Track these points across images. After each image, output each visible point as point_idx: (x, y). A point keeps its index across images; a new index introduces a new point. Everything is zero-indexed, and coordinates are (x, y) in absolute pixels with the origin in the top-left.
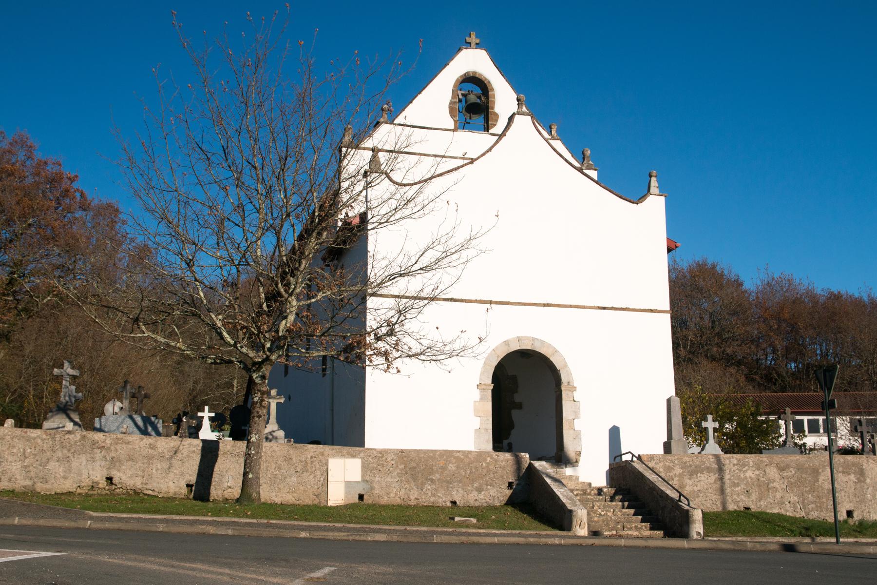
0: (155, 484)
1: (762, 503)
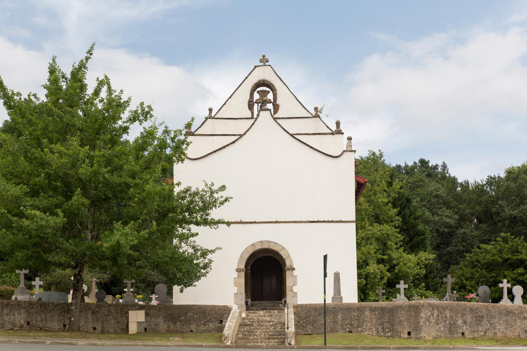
0: (49, 325)
1: (359, 329)
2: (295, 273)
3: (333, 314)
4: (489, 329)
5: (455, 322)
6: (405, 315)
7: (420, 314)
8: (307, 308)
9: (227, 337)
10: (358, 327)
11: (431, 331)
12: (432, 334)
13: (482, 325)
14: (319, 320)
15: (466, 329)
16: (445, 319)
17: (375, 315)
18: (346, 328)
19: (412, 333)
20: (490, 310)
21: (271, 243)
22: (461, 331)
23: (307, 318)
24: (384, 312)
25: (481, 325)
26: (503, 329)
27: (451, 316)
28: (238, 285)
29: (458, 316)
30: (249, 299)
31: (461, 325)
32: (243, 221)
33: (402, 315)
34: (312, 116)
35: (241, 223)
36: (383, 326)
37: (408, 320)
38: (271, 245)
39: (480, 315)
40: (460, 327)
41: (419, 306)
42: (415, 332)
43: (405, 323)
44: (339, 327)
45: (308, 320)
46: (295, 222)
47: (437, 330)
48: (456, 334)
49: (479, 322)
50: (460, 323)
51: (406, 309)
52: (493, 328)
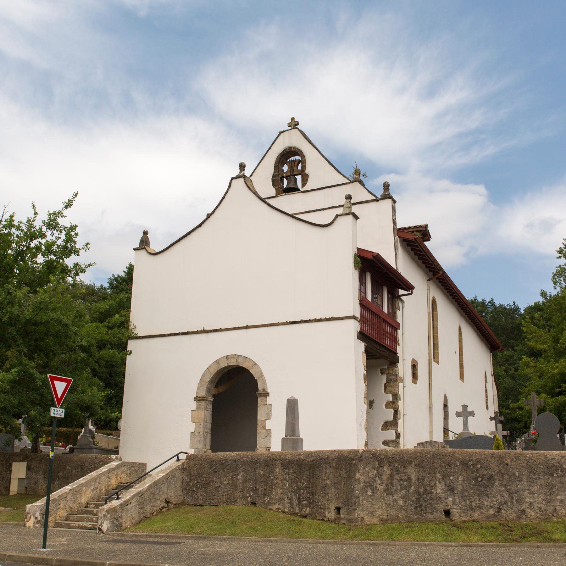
2: (269, 400)
3: (232, 472)
4: (506, 503)
5: (428, 488)
6: (331, 475)
7: (355, 474)
8: (201, 460)
9: (28, 513)
10: (265, 495)
11: (376, 506)
12: (379, 512)
13: (491, 494)
14: (213, 481)
15: (454, 503)
16: (405, 483)
17: (289, 475)
18: (248, 497)
19: (342, 511)
20: (507, 465)
21: (240, 357)
22: (442, 507)
23: (199, 477)
24: (301, 469)
25: (487, 495)
26: (540, 503)
27: (420, 477)
28: (197, 421)
29: (435, 477)
31: (442, 495)
32: (206, 329)
33: (327, 475)
34: (349, 181)
35: (204, 332)
36: (300, 495)
37: (336, 485)
38: (239, 361)
39: (484, 475)
40: (440, 498)
41: (353, 460)
42: (346, 507)
43: (331, 490)
44: (238, 494)
45: (199, 481)
46: (271, 325)
47: (390, 505)
48: (432, 514)
49: (482, 489)
50: (439, 491)
51: (334, 465)
52: (516, 500)
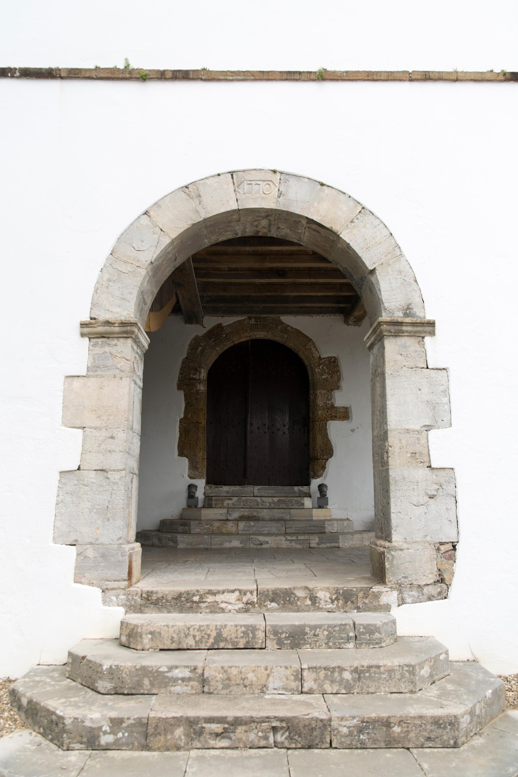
21: (292, 181)
30: (200, 477)
